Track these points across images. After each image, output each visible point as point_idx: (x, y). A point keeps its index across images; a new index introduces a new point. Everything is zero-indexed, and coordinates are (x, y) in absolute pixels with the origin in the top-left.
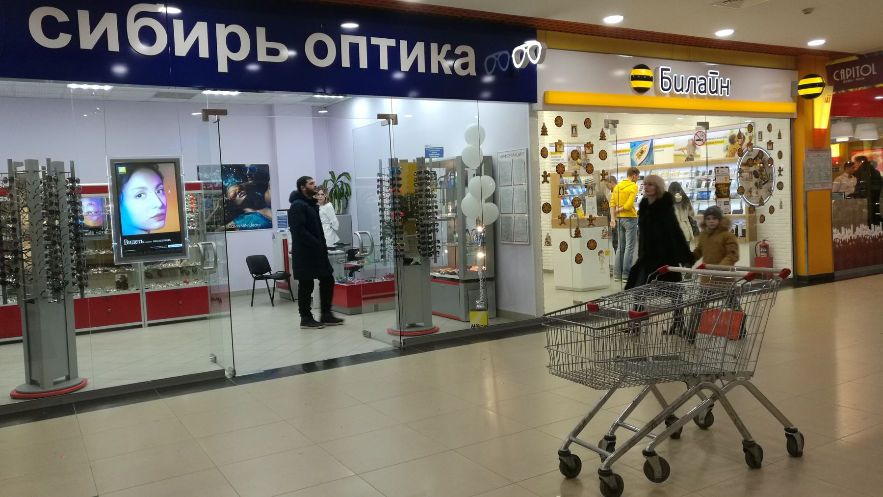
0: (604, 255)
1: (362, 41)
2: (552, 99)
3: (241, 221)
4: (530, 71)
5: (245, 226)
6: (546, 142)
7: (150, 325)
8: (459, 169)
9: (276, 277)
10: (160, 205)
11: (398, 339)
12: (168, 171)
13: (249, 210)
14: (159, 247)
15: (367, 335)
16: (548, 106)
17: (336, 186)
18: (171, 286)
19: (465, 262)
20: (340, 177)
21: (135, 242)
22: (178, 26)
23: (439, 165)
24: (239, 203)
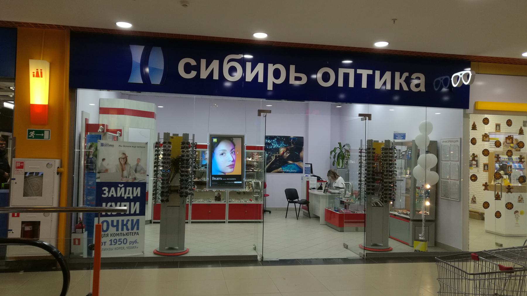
0: (519, 214)
1: (351, 72)
2: (481, 107)
3: (286, 168)
4: (464, 90)
5: (288, 171)
6: (477, 135)
7: (229, 222)
8: (413, 149)
9: (301, 203)
10: (232, 159)
11: (362, 251)
12: (238, 142)
13: (290, 162)
14: (230, 182)
15: (346, 247)
16: (477, 111)
17: (341, 151)
18: (243, 202)
19: (414, 206)
20: (344, 146)
21: (218, 179)
22: (249, 65)
23: (402, 144)
24: (285, 158)
